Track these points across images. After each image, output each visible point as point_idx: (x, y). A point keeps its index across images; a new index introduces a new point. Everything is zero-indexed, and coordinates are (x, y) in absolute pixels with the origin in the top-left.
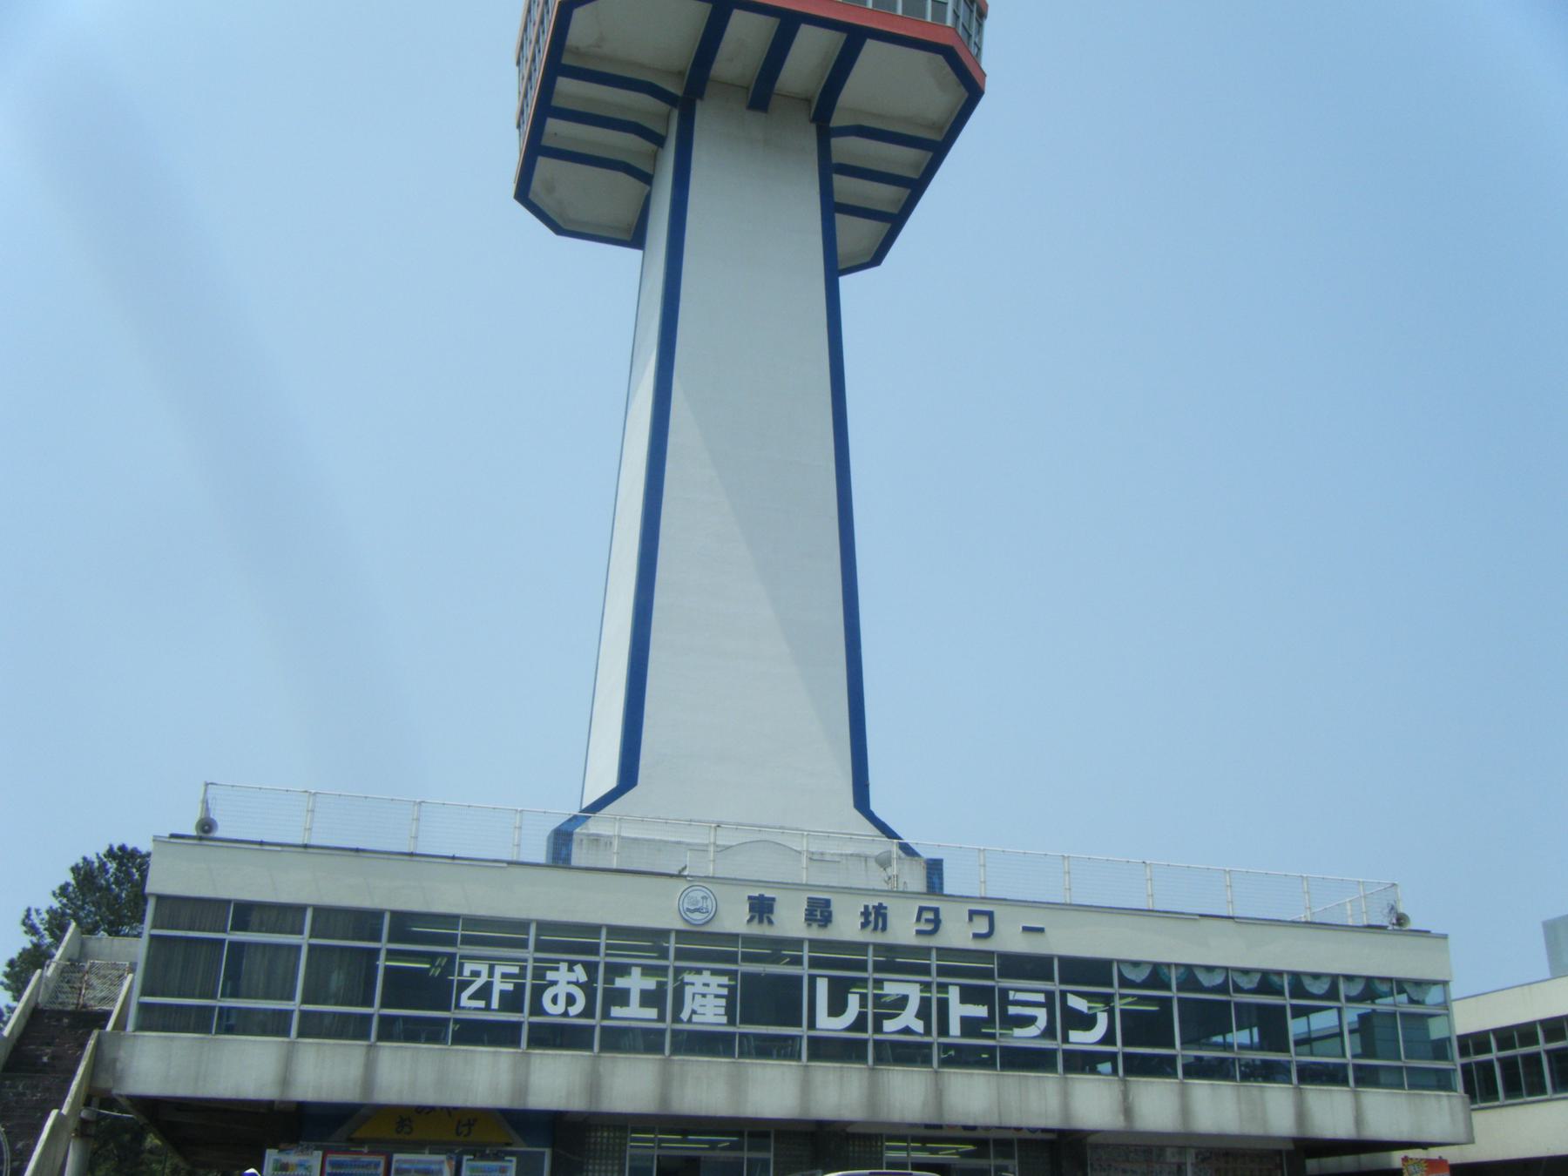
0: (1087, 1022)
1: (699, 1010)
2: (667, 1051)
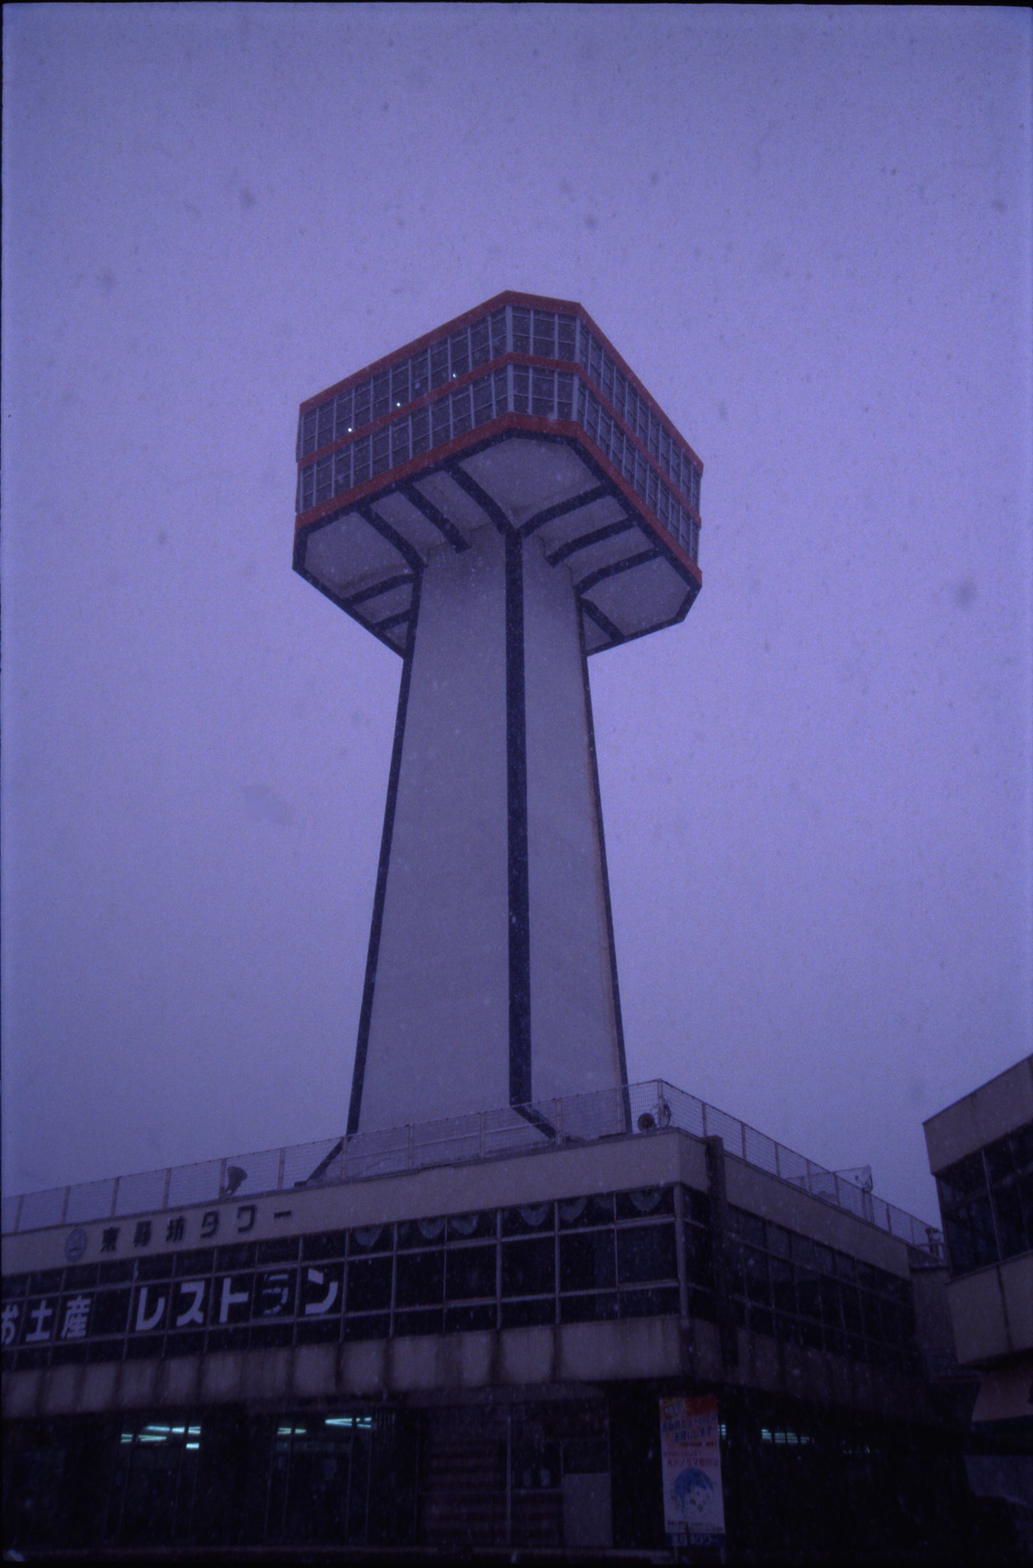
0: (318, 1293)
2: (558, 1320)
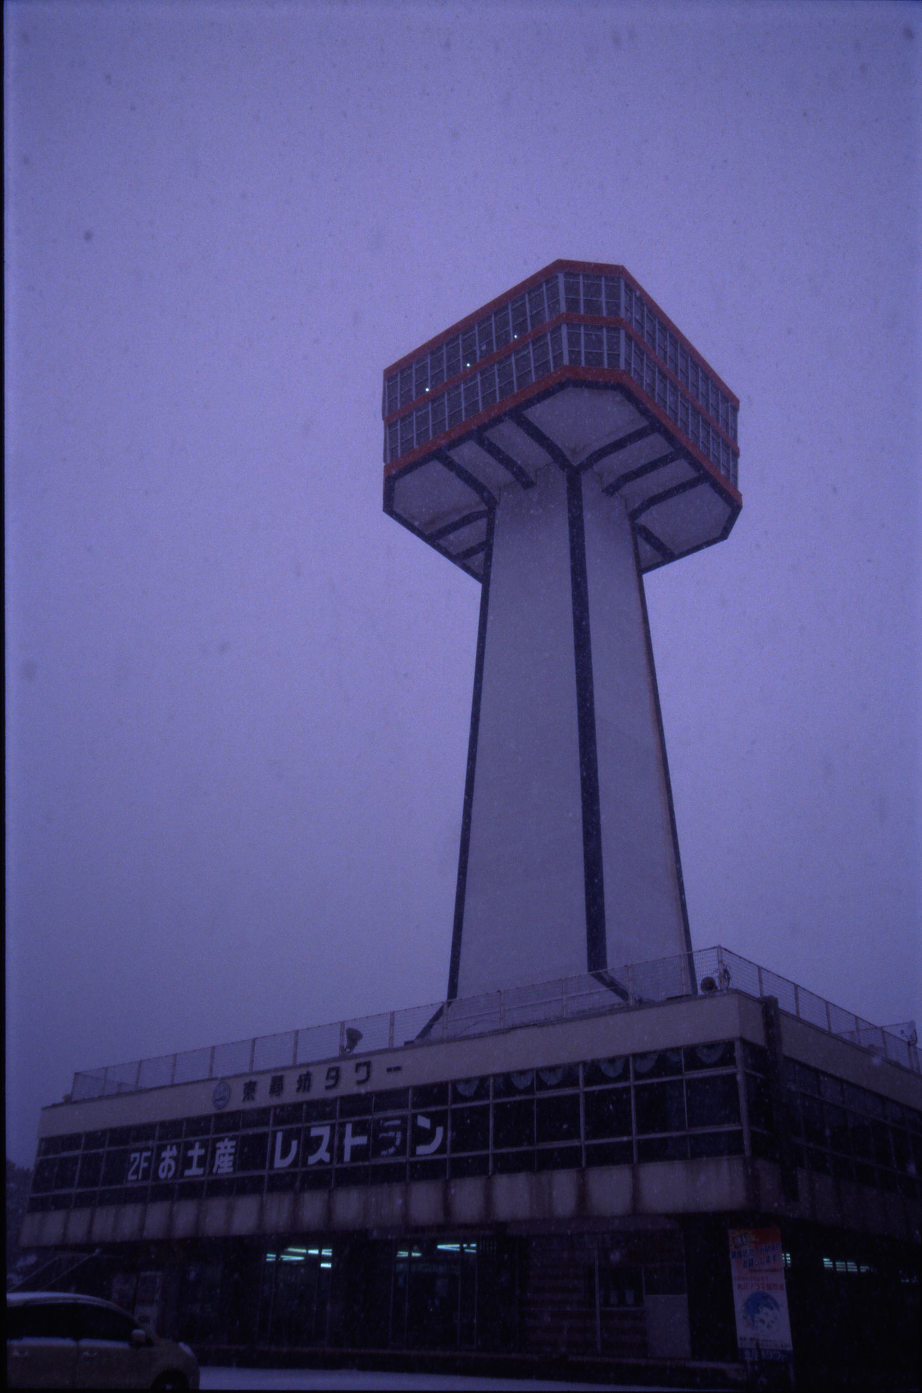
1: (221, 1165)
